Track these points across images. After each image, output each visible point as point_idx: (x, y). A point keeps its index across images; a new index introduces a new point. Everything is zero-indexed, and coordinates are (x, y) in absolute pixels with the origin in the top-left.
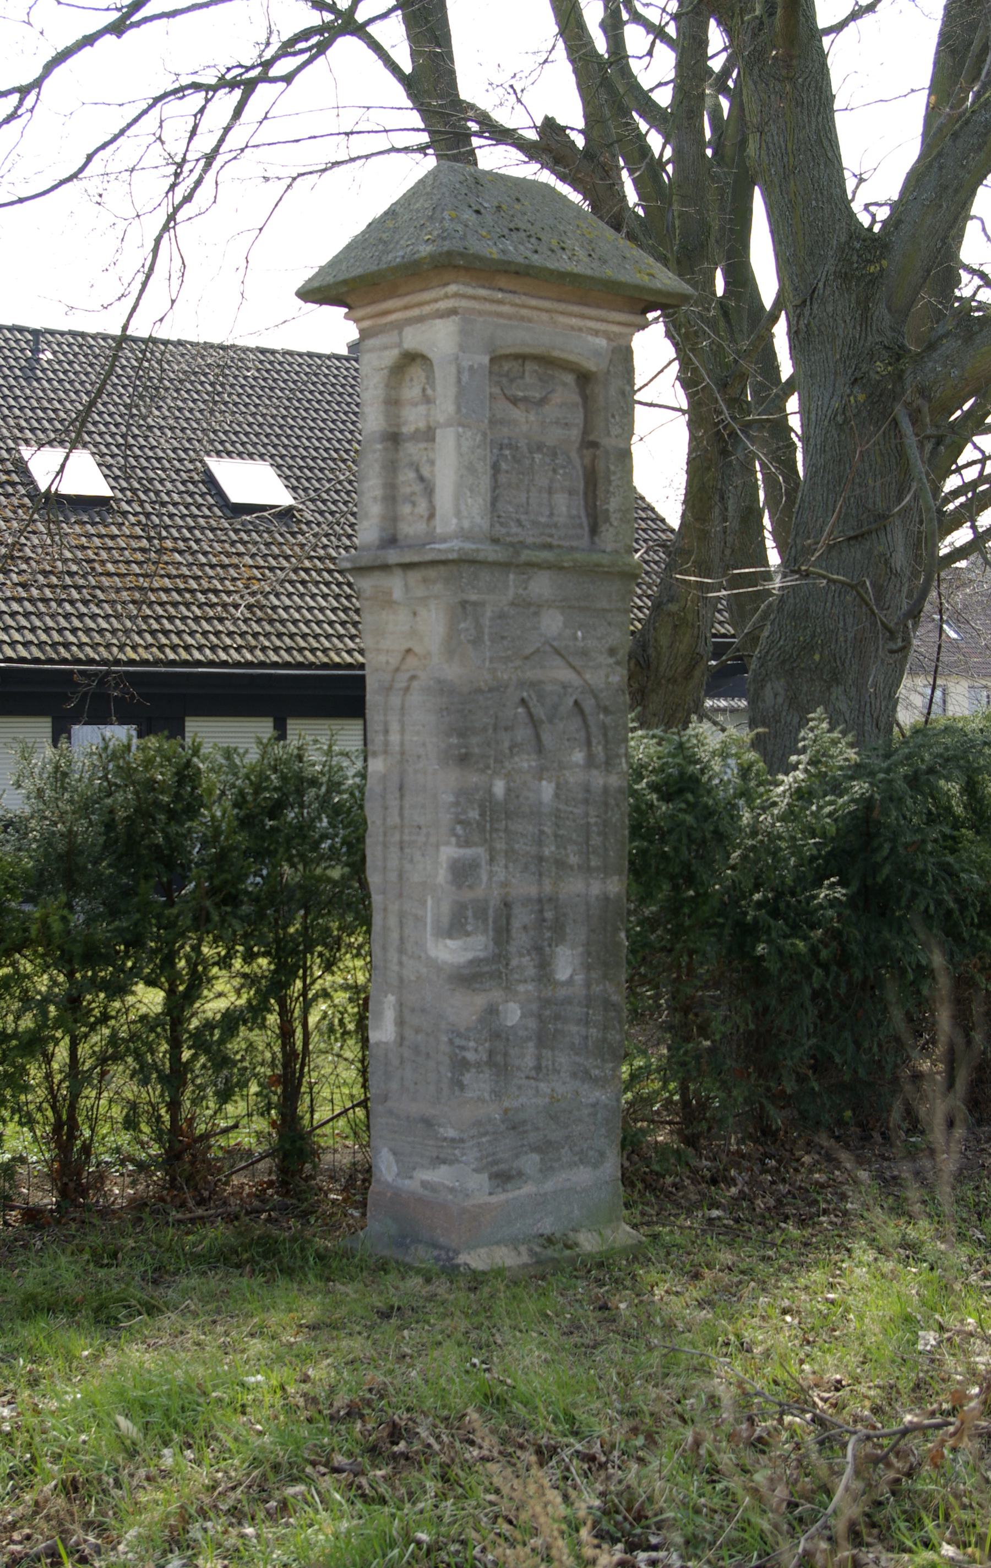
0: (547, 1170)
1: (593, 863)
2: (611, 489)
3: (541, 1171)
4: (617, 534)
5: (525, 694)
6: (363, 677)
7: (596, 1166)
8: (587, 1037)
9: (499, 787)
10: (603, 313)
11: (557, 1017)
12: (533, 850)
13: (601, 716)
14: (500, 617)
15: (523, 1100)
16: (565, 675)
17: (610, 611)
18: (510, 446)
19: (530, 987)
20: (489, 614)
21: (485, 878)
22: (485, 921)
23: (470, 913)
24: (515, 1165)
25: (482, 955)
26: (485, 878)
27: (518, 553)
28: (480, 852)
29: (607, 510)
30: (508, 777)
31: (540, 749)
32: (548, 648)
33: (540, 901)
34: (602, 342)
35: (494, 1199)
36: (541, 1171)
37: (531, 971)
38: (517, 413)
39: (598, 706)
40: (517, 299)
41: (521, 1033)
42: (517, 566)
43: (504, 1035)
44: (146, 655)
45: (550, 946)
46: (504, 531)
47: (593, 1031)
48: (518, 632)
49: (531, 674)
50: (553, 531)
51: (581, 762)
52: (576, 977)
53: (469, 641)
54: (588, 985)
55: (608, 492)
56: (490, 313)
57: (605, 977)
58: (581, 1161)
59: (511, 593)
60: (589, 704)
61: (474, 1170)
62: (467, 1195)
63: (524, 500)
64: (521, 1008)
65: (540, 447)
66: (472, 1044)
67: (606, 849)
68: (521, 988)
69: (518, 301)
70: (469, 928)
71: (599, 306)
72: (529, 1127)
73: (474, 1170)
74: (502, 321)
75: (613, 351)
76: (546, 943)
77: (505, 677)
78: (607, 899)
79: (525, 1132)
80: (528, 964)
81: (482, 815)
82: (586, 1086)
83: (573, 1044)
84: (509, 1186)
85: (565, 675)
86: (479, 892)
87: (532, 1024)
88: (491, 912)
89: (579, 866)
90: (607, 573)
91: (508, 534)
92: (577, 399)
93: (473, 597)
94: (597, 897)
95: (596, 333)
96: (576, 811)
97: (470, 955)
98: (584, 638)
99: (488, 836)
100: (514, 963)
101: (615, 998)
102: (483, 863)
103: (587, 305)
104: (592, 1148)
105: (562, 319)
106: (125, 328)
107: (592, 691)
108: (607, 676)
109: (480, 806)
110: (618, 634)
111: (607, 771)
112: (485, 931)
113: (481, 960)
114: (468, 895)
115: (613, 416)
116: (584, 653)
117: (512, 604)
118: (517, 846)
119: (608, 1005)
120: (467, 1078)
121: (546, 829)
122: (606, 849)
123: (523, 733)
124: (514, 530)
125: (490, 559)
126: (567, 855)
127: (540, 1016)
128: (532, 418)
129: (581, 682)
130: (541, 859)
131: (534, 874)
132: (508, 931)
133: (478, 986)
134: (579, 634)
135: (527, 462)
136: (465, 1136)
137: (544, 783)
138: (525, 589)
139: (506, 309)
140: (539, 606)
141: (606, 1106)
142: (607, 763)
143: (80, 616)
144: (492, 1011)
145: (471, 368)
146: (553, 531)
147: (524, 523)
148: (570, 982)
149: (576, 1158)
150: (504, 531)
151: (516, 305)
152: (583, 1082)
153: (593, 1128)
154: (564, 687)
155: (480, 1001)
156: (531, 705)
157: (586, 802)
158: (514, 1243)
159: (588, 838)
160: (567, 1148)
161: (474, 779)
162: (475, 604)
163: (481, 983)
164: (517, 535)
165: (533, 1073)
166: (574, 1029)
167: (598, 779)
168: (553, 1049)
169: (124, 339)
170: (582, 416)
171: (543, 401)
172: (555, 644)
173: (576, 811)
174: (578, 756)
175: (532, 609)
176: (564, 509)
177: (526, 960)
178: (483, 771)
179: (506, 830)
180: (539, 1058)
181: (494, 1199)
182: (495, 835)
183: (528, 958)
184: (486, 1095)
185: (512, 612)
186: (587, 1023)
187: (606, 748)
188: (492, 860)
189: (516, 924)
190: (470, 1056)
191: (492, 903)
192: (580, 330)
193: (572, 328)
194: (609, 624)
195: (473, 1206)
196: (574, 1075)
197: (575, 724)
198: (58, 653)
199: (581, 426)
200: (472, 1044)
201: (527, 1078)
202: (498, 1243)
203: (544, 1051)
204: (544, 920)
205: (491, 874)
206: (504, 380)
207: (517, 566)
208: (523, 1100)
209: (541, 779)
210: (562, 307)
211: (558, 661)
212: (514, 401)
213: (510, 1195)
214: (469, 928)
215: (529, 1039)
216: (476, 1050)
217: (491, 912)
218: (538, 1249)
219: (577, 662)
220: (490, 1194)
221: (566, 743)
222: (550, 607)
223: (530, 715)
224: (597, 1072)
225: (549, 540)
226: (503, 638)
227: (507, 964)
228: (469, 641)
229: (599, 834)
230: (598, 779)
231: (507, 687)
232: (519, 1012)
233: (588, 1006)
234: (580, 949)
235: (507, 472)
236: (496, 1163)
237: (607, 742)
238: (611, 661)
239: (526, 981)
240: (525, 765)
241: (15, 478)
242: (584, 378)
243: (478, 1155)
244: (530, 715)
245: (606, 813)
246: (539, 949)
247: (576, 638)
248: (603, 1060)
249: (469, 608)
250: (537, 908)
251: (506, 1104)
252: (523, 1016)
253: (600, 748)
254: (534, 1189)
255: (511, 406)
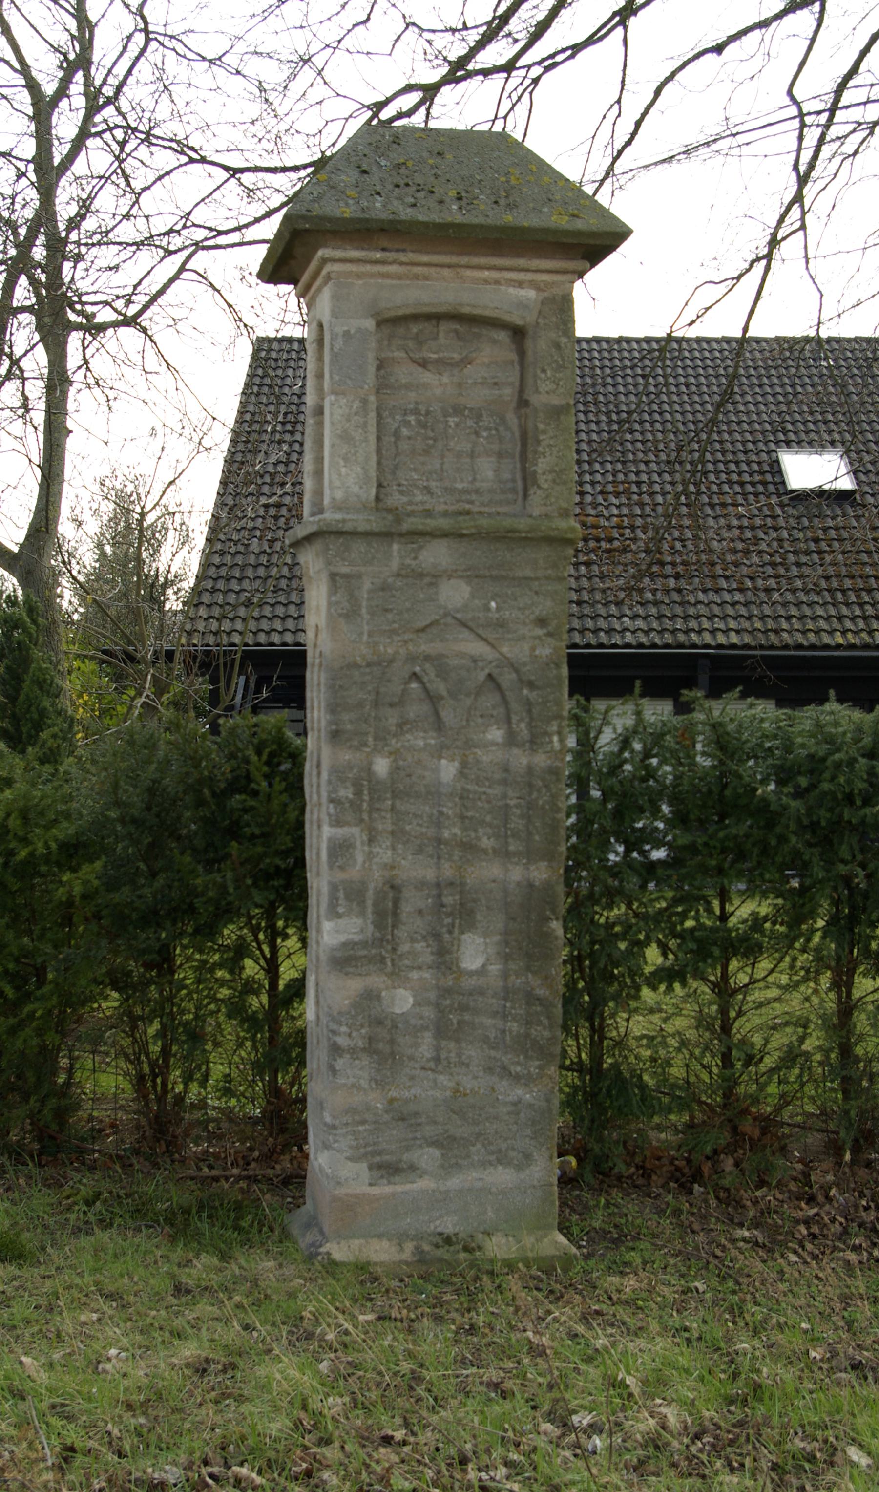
0: (450, 1167)
1: (511, 848)
2: (540, 449)
3: (442, 1166)
4: (547, 497)
5: (417, 669)
6: (305, 651)
7: (519, 1168)
8: (503, 1032)
9: (382, 766)
10: (521, 262)
11: (463, 1008)
12: (432, 832)
13: (525, 692)
14: (383, 589)
15: (416, 1091)
16: (477, 648)
17: (537, 579)
18: (416, 412)
19: (426, 975)
20: (367, 585)
21: (360, 858)
22: (362, 903)
23: (341, 894)
24: (405, 1157)
25: (357, 938)
26: (360, 858)
27: (398, 520)
28: (355, 832)
29: (535, 472)
30: (395, 754)
31: (439, 725)
32: (449, 620)
33: (438, 885)
34: (531, 294)
35: (375, 1191)
36: (442, 1166)
37: (427, 958)
38: (427, 377)
39: (521, 681)
40: (402, 257)
41: (413, 1022)
42: (401, 535)
43: (388, 1023)
44: (856, 641)
45: (450, 932)
46: (405, 499)
47: (514, 1026)
48: (408, 605)
49: (425, 647)
50: (474, 497)
51: (500, 740)
52: (491, 968)
53: (340, 615)
54: (505, 975)
55: (535, 452)
56: (372, 275)
57: (528, 968)
58: (499, 1161)
59: (395, 564)
60: (507, 678)
61: (347, 1158)
62: (339, 1183)
63: (438, 466)
64: (414, 996)
65: (458, 410)
66: (344, 1029)
67: (530, 834)
68: (415, 975)
69: (404, 259)
70: (341, 910)
71: (519, 255)
72: (423, 1119)
73: (347, 1158)
74: (388, 282)
75: (542, 303)
76: (445, 930)
77: (390, 651)
78: (531, 885)
79: (419, 1124)
80: (424, 952)
81: (358, 793)
82: (505, 1083)
83: (488, 1037)
84: (397, 1179)
85: (477, 648)
86: (354, 873)
87: (429, 1013)
88: (370, 894)
89: (495, 851)
90: (526, 538)
91: (410, 503)
92: (514, 356)
93: (345, 570)
94: (518, 884)
95: (520, 284)
96: (489, 791)
97: (343, 938)
98: (498, 609)
99: (365, 816)
100: (405, 948)
101: (540, 992)
102: (358, 843)
103: (501, 255)
104: (513, 1149)
105: (468, 273)
106: (745, 329)
107: (512, 665)
108: (533, 649)
109: (353, 785)
110: (549, 603)
111: (532, 750)
112: (362, 913)
113: (356, 944)
114: (340, 876)
115: (544, 371)
116: (501, 624)
117: (398, 575)
118: (408, 828)
119: (530, 998)
120: (340, 1063)
121: (445, 810)
122: (530, 834)
123: (416, 709)
124: (419, 498)
125: (361, 529)
126: (478, 839)
127: (437, 1005)
128: (445, 379)
129: (497, 655)
130: (439, 841)
131: (431, 856)
132: (395, 914)
133: (351, 970)
134: (493, 604)
135: (442, 426)
136: (337, 1122)
137: (444, 762)
138: (415, 558)
139: (393, 269)
140: (434, 576)
141: (531, 1105)
142: (532, 742)
143: (798, 604)
144: (371, 996)
145: (347, 334)
146: (474, 497)
147: (435, 490)
148: (482, 971)
149: (493, 1158)
150: (405, 499)
151: (402, 264)
152: (502, 1077)
153: (514, 1128)
154: (475, 661)
155: (355, 985)
156: (425, 679)
157: (504, 782)
158: (400, 1238)
159: (506, 821)
160: (479, 1146)
161: (347, 756)
162: (346, 576)
163: (356, 967)
164: (422, 503)
165: (432, 1064)
166: (488, 1022)
167: (520, 759)
168: (458, 1041)
169: (744, 341)
170: (517, 373)
171: (465, 362)
172: (459, 616)
173: (489, 791)
174: (496, 734)
175: (427, 580)
176: (490, 474)
177: (419, 946)
178: (357, 749)
179: (393, 808)
180: (438, 1049)
181: (375, 1191)
182: (375, 815)
183: (424, 944)
184: (364, 1083)
185: (399, 583)
186: (505, 1017)
187: (530, 726)
188: (371, 841)
189: (406, 908)
190: (342, 1041)
191: (371, 886)
192: (497, 282)
193: (486, 282)
194: (537, 593)
195: (347, 1195)
196: (489, 1070)
197: (489, 700)
198: (767, 639)
199: (517, 384)
200: (344, 1029)
201: (423, 1068)
202: (380, 1236)
203: (444, 1043)
204: (443, 906)
205: (370, 856)
206: (411, 344)
207: (401, 535)
208: (416, 1091)
209: (440, 757)
210: (464, 260)
211: (466, 634)
212: (423, 364)
213: (399, 1188)
214: (341, 910)
215: (425, 1028)
216: (350, 1035)
217: (370, 894)
218: (426, 1247)
219: (491, 635)
220: (371, 1185)
221: (479, 720)
222: (450, 577)
223: (426, 690)
224: (518, 1069)
225: (467, 506)
226: (386, 610)
227: (394, 950)
228: (340, 615)
229: (522, 816)
230: (520, 759)
231: (391, 661)
232: (411, 1000)
233: (505, 999)
234: (497, 938)
235: (409, 438)
236: (375, 1153)
237: (532, 719)
238: (540, 632)
239: (420, 968)
240: (421, 743)
241: (768, 477)
242: (518, 333)
243: (354, 1143)
244: (426, 690)
245: (530, 794)
246: (437, 936)
247: (487, 609)
248: (526, 1057)
249: (340, 581)
250: (434, 892)
251: (393, 1093)
252: (417, 1004)
253: (523, 725)
254: (433, 1185)
255: (420, 369)
